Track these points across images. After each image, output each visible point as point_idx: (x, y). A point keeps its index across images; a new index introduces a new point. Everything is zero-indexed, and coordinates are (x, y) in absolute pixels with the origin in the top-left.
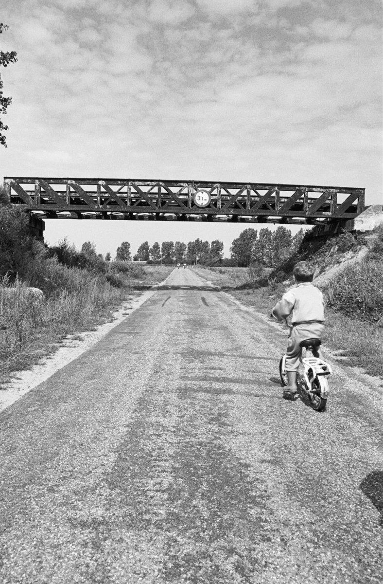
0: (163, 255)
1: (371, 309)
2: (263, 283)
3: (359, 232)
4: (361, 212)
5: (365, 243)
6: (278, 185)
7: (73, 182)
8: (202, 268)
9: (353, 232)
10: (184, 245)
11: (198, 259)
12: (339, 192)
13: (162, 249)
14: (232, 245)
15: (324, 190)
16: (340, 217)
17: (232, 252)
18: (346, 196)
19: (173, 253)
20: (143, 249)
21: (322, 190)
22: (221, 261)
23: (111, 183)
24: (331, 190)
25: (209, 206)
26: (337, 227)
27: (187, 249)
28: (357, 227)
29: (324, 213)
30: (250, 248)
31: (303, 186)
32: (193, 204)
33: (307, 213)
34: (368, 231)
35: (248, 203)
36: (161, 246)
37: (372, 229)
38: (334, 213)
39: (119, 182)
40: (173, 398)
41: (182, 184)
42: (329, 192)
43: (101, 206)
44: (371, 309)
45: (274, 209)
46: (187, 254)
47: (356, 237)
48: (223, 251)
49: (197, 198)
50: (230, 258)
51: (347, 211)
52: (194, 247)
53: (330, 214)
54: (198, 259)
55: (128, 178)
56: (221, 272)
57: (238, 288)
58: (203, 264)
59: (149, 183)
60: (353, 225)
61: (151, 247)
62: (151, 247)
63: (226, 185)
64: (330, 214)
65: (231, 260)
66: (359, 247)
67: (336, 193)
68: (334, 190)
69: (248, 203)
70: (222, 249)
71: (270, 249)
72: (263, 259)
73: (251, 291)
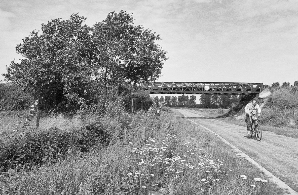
0: (166, 102)
1: (262, 122)
2: (227, 115)
3: (261, 98)
4: (262, 91)
5: (263, 102)
6: (232, 83)
7: (164, 83)
8: (188, 109)
9: (259, 98)
10: (176, 97)
11: (183, 104)
12: (254, 85)
13: (165, 100)
14: (200, 98)
15: (248, 84)
16: (254, 93)
17: (201, 101)
18: (257, 86)
19: (171, 101)
20: (156, 100)
21: (248, 84)
22: (195, 105)
23: (177, 83)
24: (251, 84)
25: (209, 90)
26: (253, 96)
27: (178, 99)
28: (261, 96)
29: (248, 92)
30: (210, 98)
31: (241, 83)
32: (204, 90)
33: (243, 92)
34: (264, 98)
35: (222, 89)
36: (164, 98)
37: (265, 97)
38: (252, 92)
39: (179, 83)
40: (260, 102)
41: (200, 83)
42: (250, 84)
43: (173, 91)
44: (262, 122)
45: (231, 91)
46: (178, 102)
47: (260, 100)
48: (196, 100)
49: (205, 88)
50: (200, 104)
51: (257, 91)
52: (181, 98)
53: (250, 92)
54: (183, 104)
55: (182, 82)
56: (201, 111)
57: (217, 118)
58: (186, 106)
59: (189, 83)
60: (259, 96)
61: (159, 99)
62: (159, 99)
63: (215, 83)
64: (250, 92)
65: (200, 105)
66: (261, 103)
67: (253, 85)
68: (252, 84)
69: (222, 89)
70: (196, 99)
71: (220, 99)
72: (216, 104)
73: (223, 118)
